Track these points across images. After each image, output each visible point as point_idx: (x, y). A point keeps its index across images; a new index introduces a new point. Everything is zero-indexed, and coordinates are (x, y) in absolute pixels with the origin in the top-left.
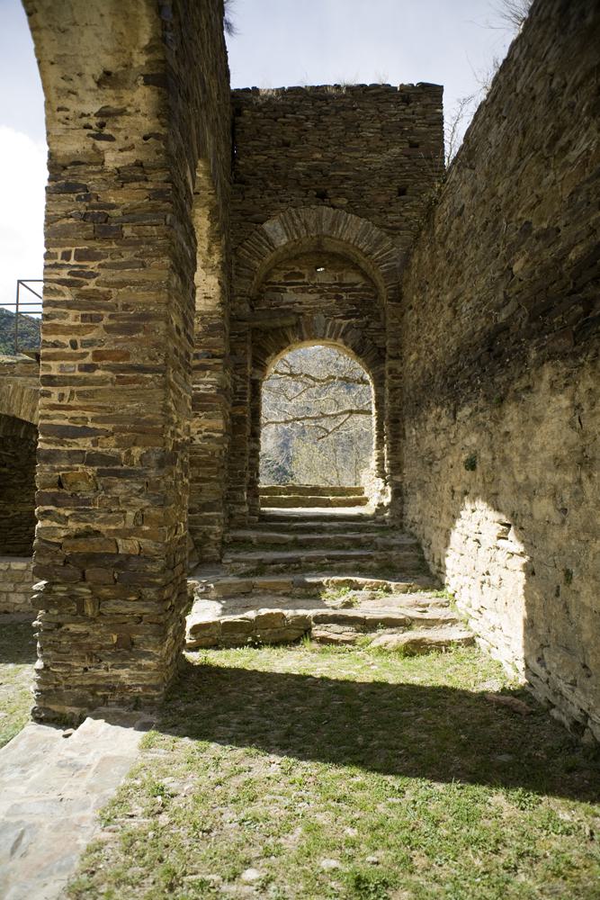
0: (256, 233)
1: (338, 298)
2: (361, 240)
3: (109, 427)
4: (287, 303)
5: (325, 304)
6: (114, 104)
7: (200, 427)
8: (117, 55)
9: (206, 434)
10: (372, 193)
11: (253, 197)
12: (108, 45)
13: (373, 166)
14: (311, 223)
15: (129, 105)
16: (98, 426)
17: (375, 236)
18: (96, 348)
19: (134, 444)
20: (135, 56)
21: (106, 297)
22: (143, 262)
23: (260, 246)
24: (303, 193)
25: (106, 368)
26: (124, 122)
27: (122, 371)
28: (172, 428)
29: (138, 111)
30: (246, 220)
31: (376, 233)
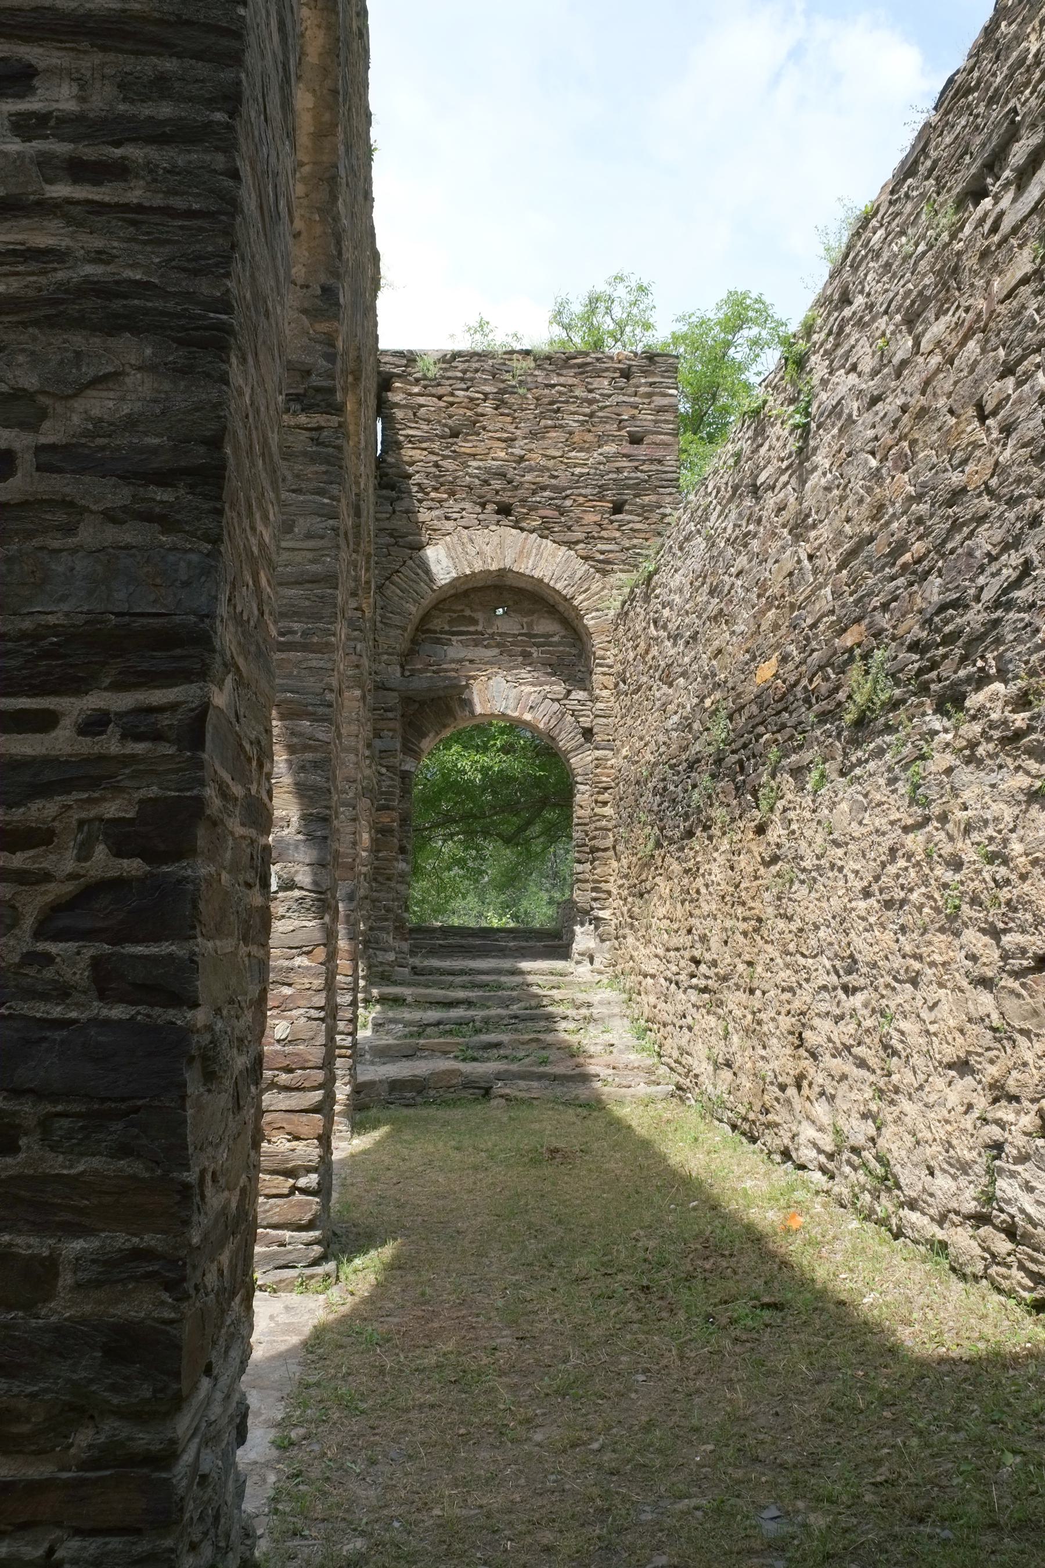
4: (453, 661)
13: (577, 470)
14: (487, 549)
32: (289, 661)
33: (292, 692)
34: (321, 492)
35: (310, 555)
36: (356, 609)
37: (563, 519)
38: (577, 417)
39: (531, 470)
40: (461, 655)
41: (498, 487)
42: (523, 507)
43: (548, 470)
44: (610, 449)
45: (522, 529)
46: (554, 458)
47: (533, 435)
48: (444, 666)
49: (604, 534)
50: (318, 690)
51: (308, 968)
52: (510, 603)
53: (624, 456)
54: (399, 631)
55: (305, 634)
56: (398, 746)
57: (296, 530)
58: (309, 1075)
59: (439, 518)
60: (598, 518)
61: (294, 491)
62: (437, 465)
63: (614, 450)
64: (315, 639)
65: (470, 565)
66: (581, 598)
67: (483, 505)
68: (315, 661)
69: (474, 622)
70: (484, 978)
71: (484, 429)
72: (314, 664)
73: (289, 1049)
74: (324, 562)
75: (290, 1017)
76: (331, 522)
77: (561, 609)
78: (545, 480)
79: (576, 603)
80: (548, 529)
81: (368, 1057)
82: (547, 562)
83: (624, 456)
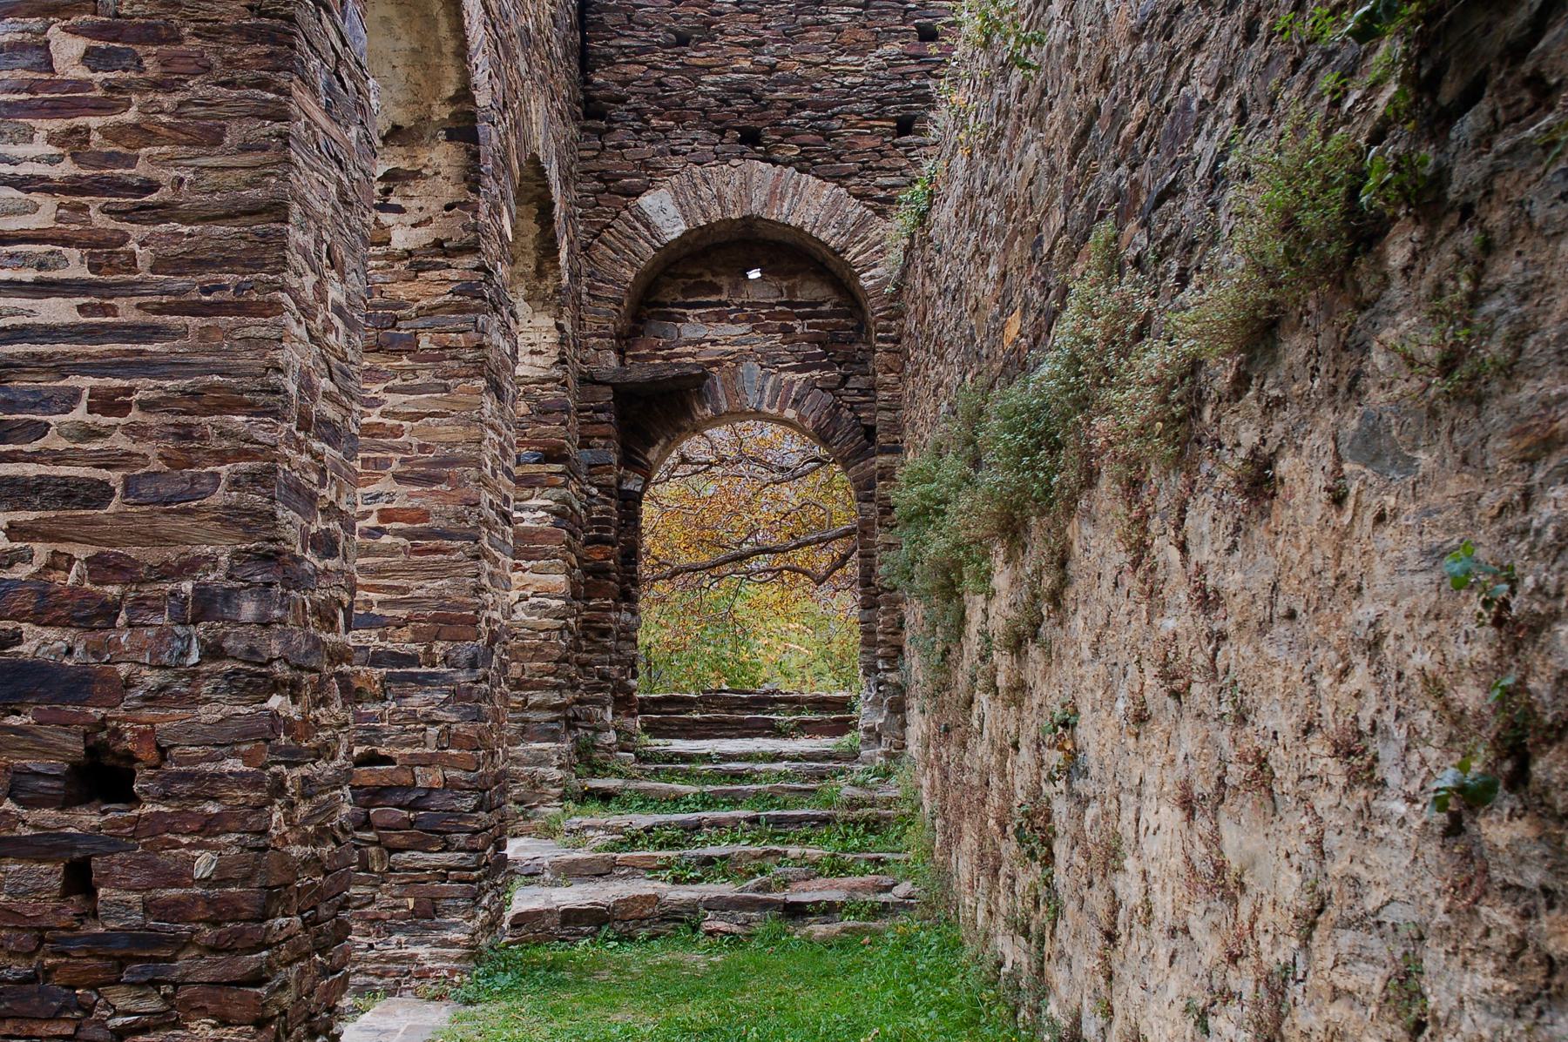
0: (626, 213)
1: (787, 331)
2: (826, 226)
3: (402, 613)
4: (689, 343)
5: (761, 342)
6: (404, 165)
7: (524, 587)
8: (412, 108)
9: (534, 600)
10: (849, 133)
11: (621, 146)
12: (400, 97)
13: (848, 80)
14: (729, 193)
15: (426, 166)
16: (388, 613)
17: (852, 218)
18: (381, 505)
19: (437, 638)
20: (436, 108)
21: (396, 432)
22: (446, 385)
23: (634, 240)
24: (715, 138)
25: (398, 533)
26: (416, 189)
27: (420, 537)
28: (487, 614)
29: (437, 174)
30: (607, 189)
31: (854, 209)
32: (217, 328)
33: (221, 374)
34: (263, 84)
35: (246, 175)
36: (477, 269)
37: (829, 146)
38: (846, 9)
39: (785, 82)
40: (700, 335)
41: (740, 108)
42: (774, 132)
43: (808, 80)
44: (893, 48)
45: (775, 163)
46: (816, 65)
47: (787, 36)
48: (678, 350)
49: (884, 162)
50: (258, 370)
51: (242, 774)
52: (764, 262)
53: (912, 57)
54: (612, 306)
55: (239, 288)
56: (614, 458)
57: (227, 140)
58: (242, 932)
59: (662, 153)
60: (877, 142)
61: (223, 84)
62: (659, 83)
63: (897, 50)
64: (254, 297)
65: (704, 212)
66: (855, 251)
67: (722, 133)
68: (256, 327)
69: (718, 290)
70: (733, 765)
71: (722, 32)
72: (252, 332)
73: (215, 892)
74: (267, 185)
75: (217, 847)
76: (277, 126)
77: (833, 267)
78: (804, 96)
79: (848, 257)
80: (809, 160)
81: (547, 875)
82: (808, 204)
83: (912, 57)
